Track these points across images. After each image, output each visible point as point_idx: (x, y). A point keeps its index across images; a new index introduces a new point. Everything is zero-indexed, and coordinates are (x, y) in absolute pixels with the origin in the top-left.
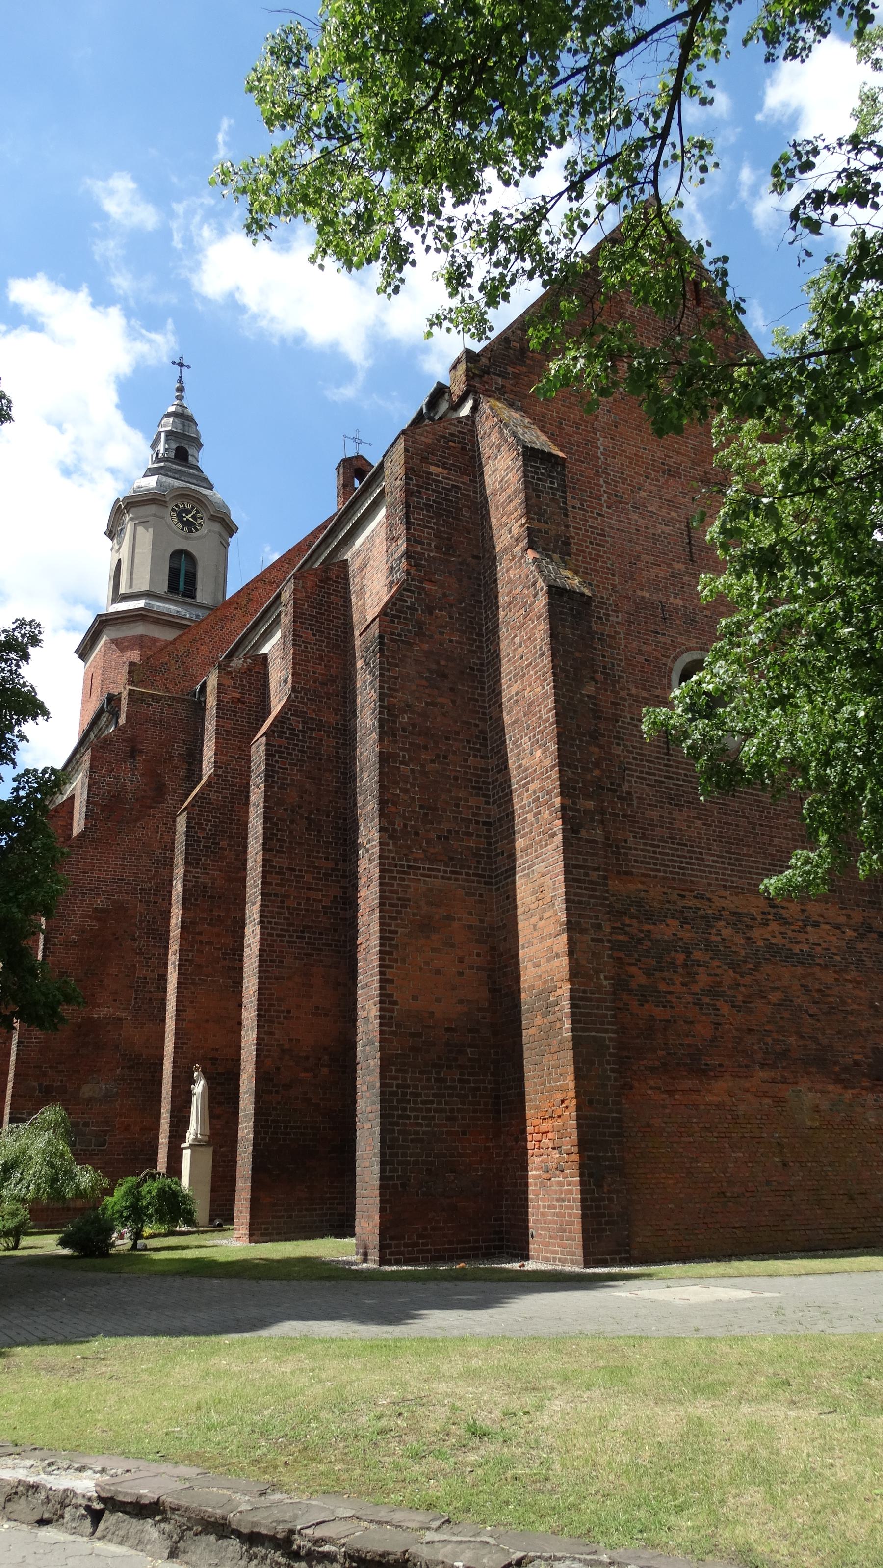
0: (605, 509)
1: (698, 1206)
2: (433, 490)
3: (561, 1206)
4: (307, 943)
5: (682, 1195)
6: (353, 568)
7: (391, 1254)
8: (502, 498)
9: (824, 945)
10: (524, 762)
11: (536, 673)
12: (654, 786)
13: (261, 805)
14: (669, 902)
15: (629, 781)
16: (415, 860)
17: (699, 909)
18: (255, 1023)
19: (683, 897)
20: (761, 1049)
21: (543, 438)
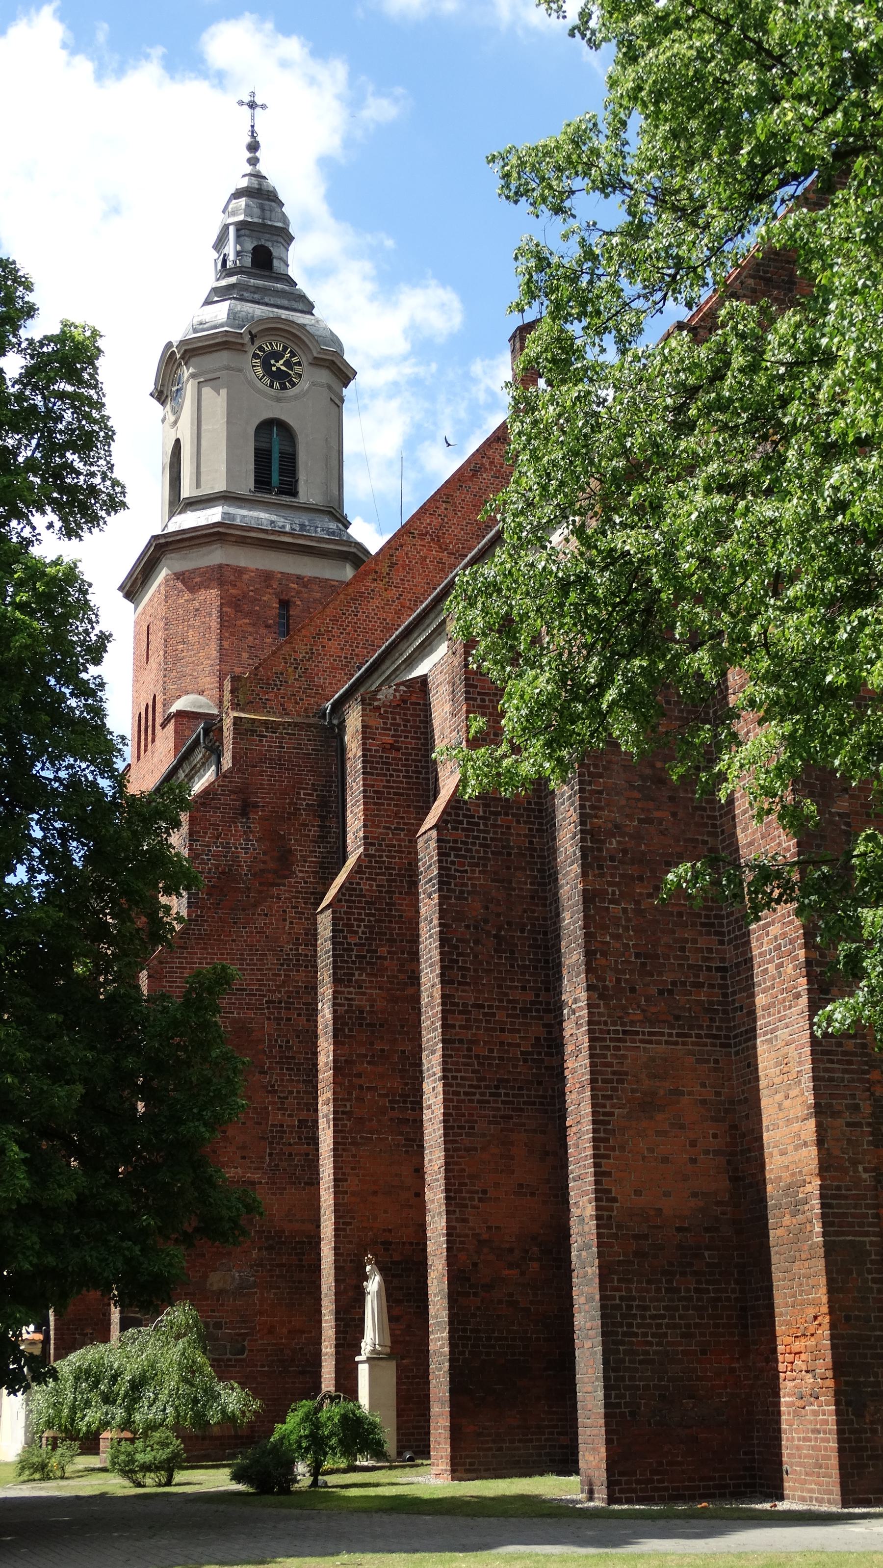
3: (816, 1438)
4: (503, 1102)
13: (436, 922)
16: (632, 1023)
18: (444, 1207)
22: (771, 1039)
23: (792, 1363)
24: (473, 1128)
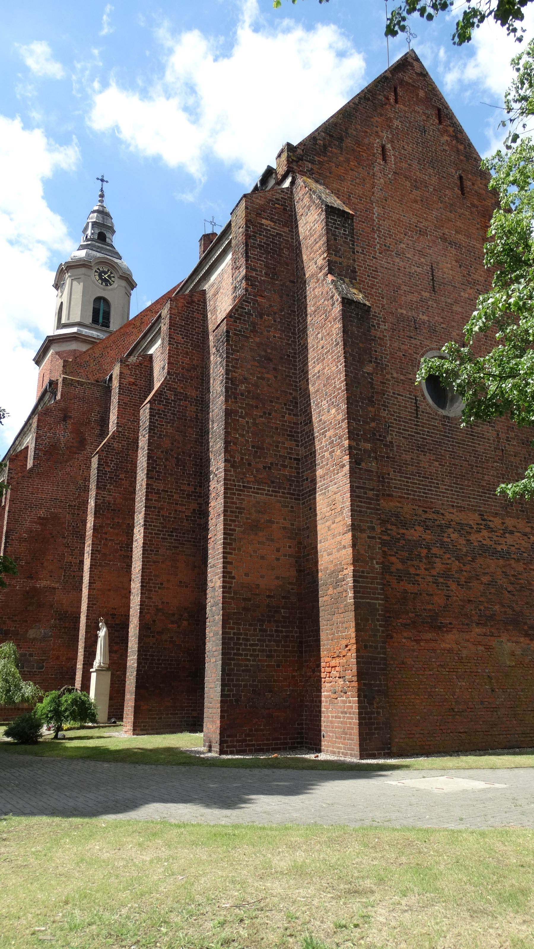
0: (378, 254)
1: (435, 717)
2: (264, 236)
3: (344, 717)
5: (425, 711)
6: (209, 295)
7: (228, 747)
8: (310, 242)
9: (517, 546)
10: (323, 418)
11: (332, 357)
12: (408, 439)
13: (146, 448)
14: (416, 515)
15: (392, 435)
16: (248, 482)
17: (436, 520)
18: (140, 591)
19: (426, 512)
20: (476, 613)
21: (339, 202)
22: (325, 493)
23: (330, 673)
24: (158, 551)
